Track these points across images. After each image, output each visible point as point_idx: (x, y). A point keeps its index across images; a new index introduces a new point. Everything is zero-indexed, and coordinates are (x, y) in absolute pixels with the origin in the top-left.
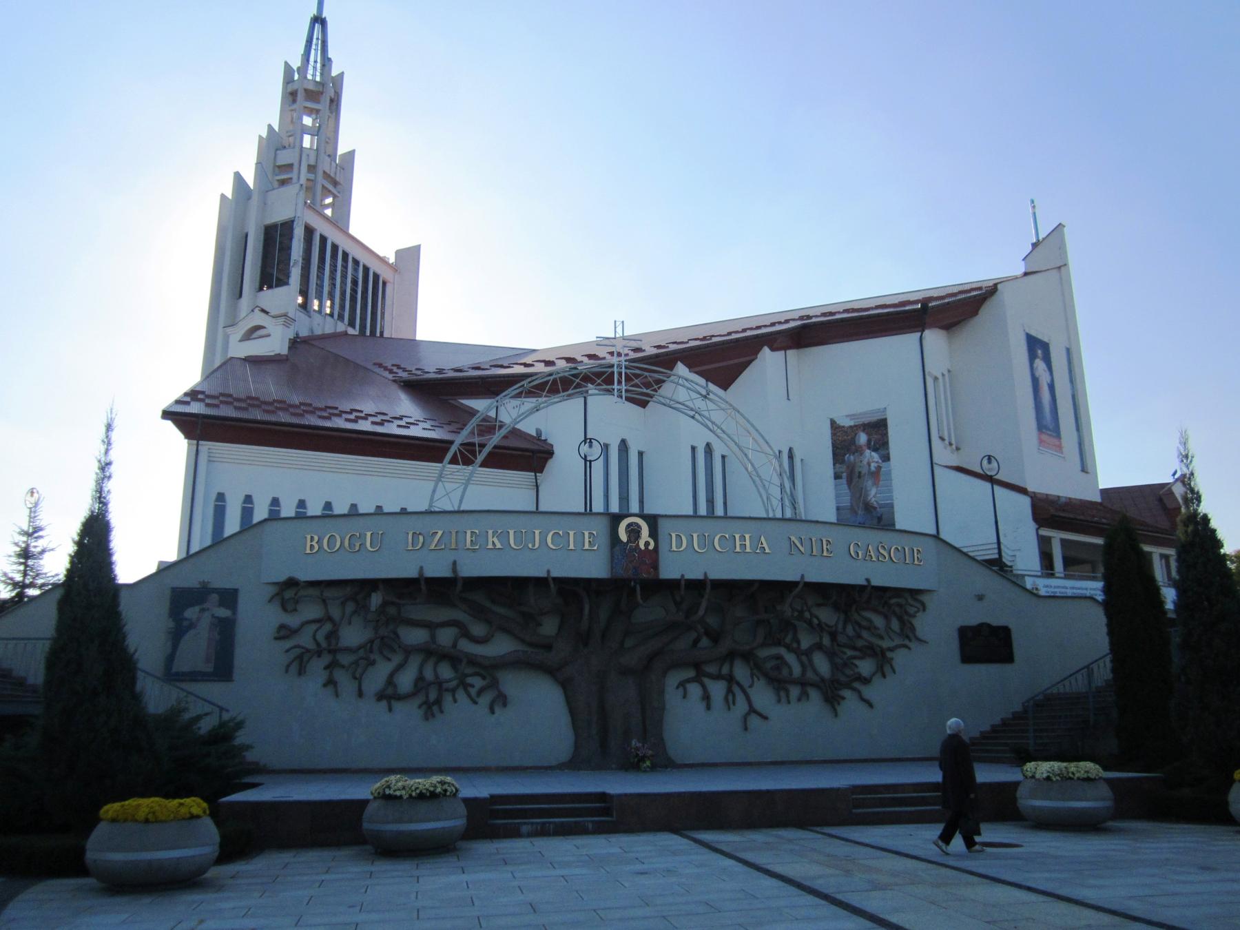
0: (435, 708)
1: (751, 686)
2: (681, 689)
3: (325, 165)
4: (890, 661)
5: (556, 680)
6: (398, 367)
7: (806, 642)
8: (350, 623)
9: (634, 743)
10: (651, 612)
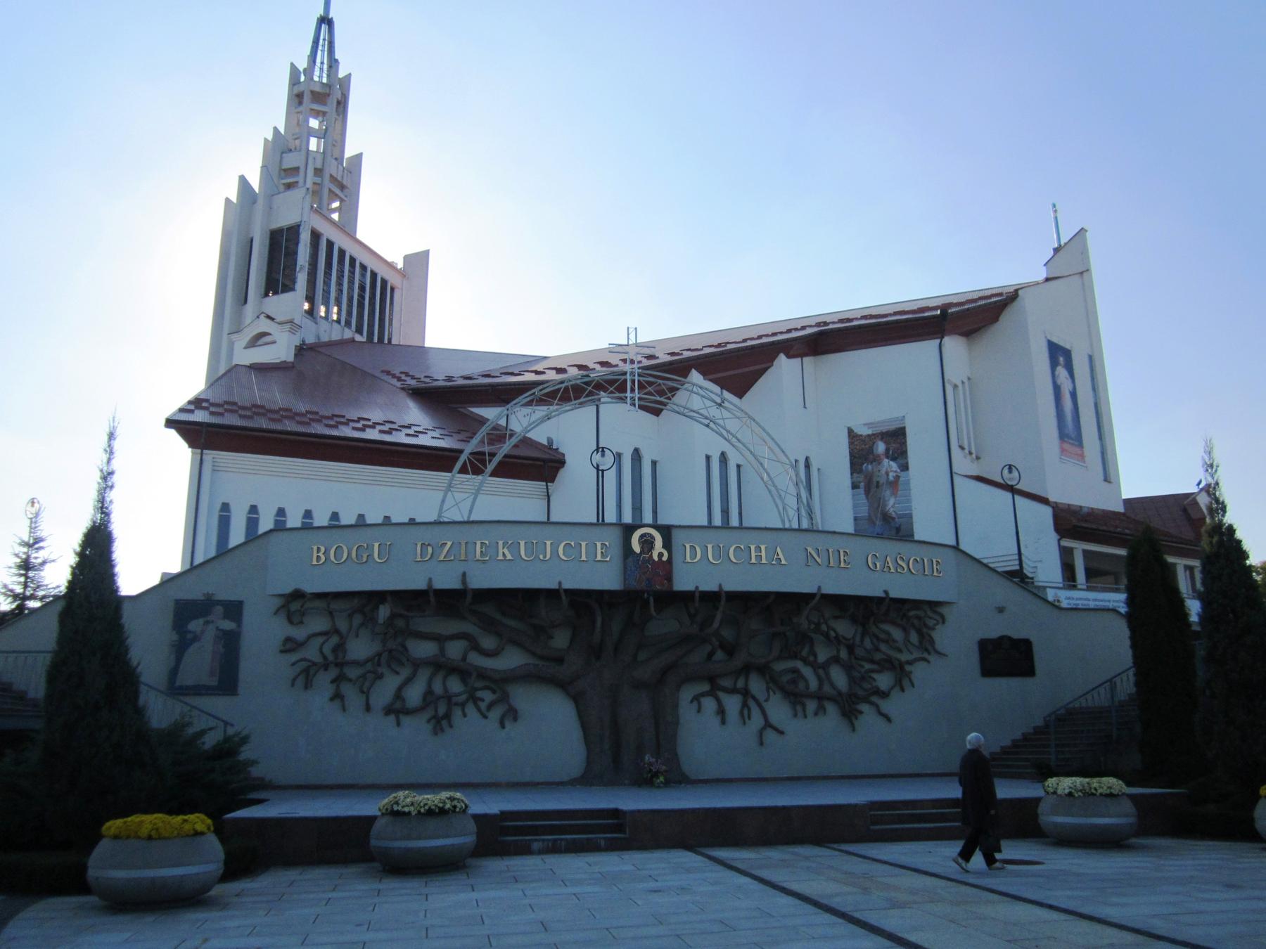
0: (444, 723)
1: (766, 700)
2: (695, 703)
3: (332, 169)
4: (908, 674)
5: (568, 694)
6: (407, 374)
7: (823, 655)
8: (357, 636)
9: (647, 758)
10: (665, 625)
